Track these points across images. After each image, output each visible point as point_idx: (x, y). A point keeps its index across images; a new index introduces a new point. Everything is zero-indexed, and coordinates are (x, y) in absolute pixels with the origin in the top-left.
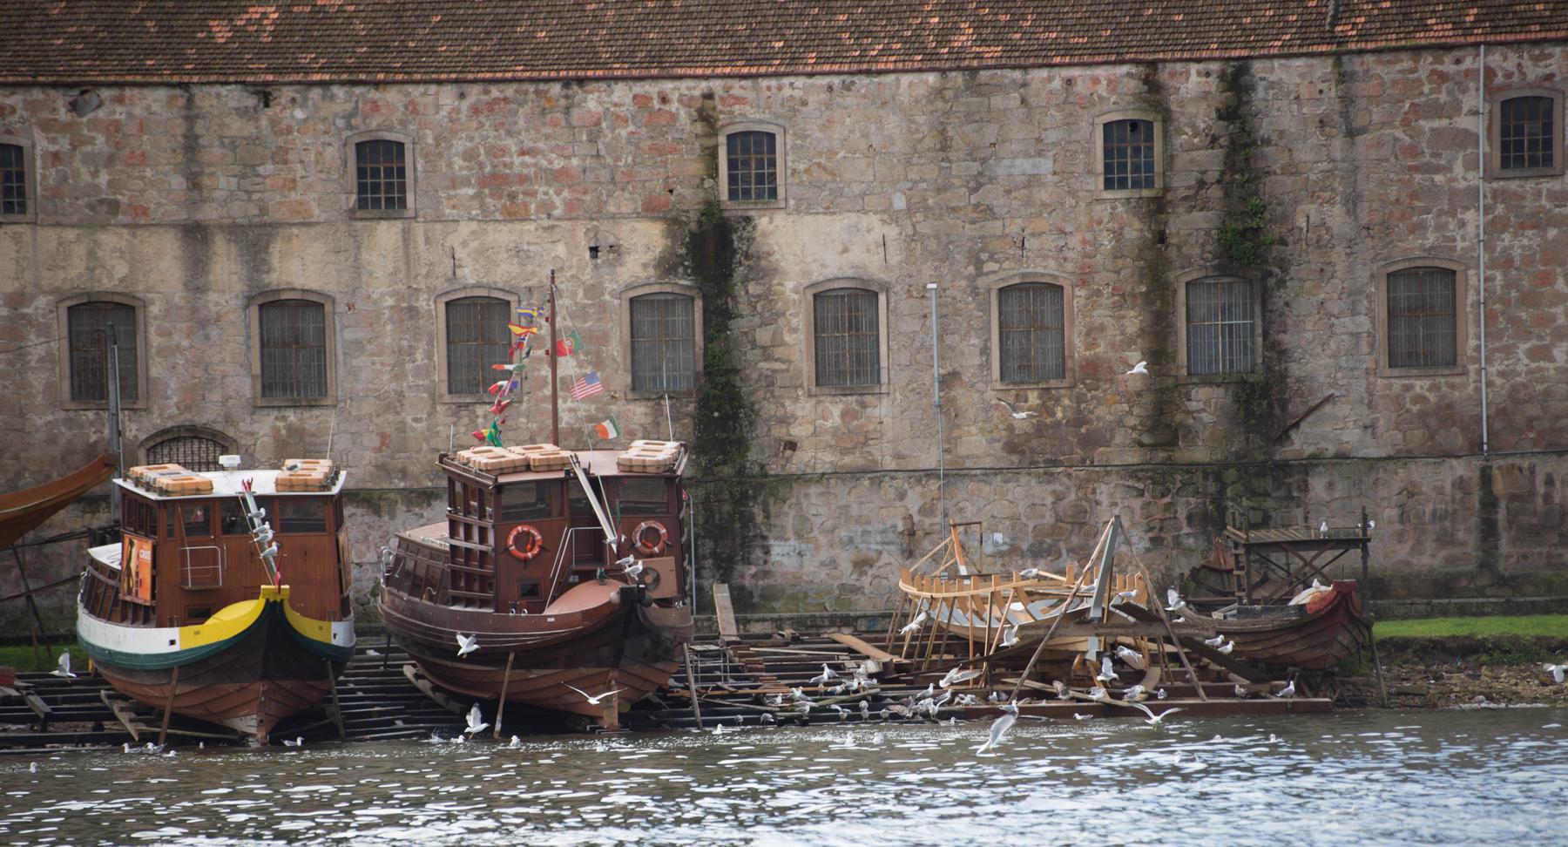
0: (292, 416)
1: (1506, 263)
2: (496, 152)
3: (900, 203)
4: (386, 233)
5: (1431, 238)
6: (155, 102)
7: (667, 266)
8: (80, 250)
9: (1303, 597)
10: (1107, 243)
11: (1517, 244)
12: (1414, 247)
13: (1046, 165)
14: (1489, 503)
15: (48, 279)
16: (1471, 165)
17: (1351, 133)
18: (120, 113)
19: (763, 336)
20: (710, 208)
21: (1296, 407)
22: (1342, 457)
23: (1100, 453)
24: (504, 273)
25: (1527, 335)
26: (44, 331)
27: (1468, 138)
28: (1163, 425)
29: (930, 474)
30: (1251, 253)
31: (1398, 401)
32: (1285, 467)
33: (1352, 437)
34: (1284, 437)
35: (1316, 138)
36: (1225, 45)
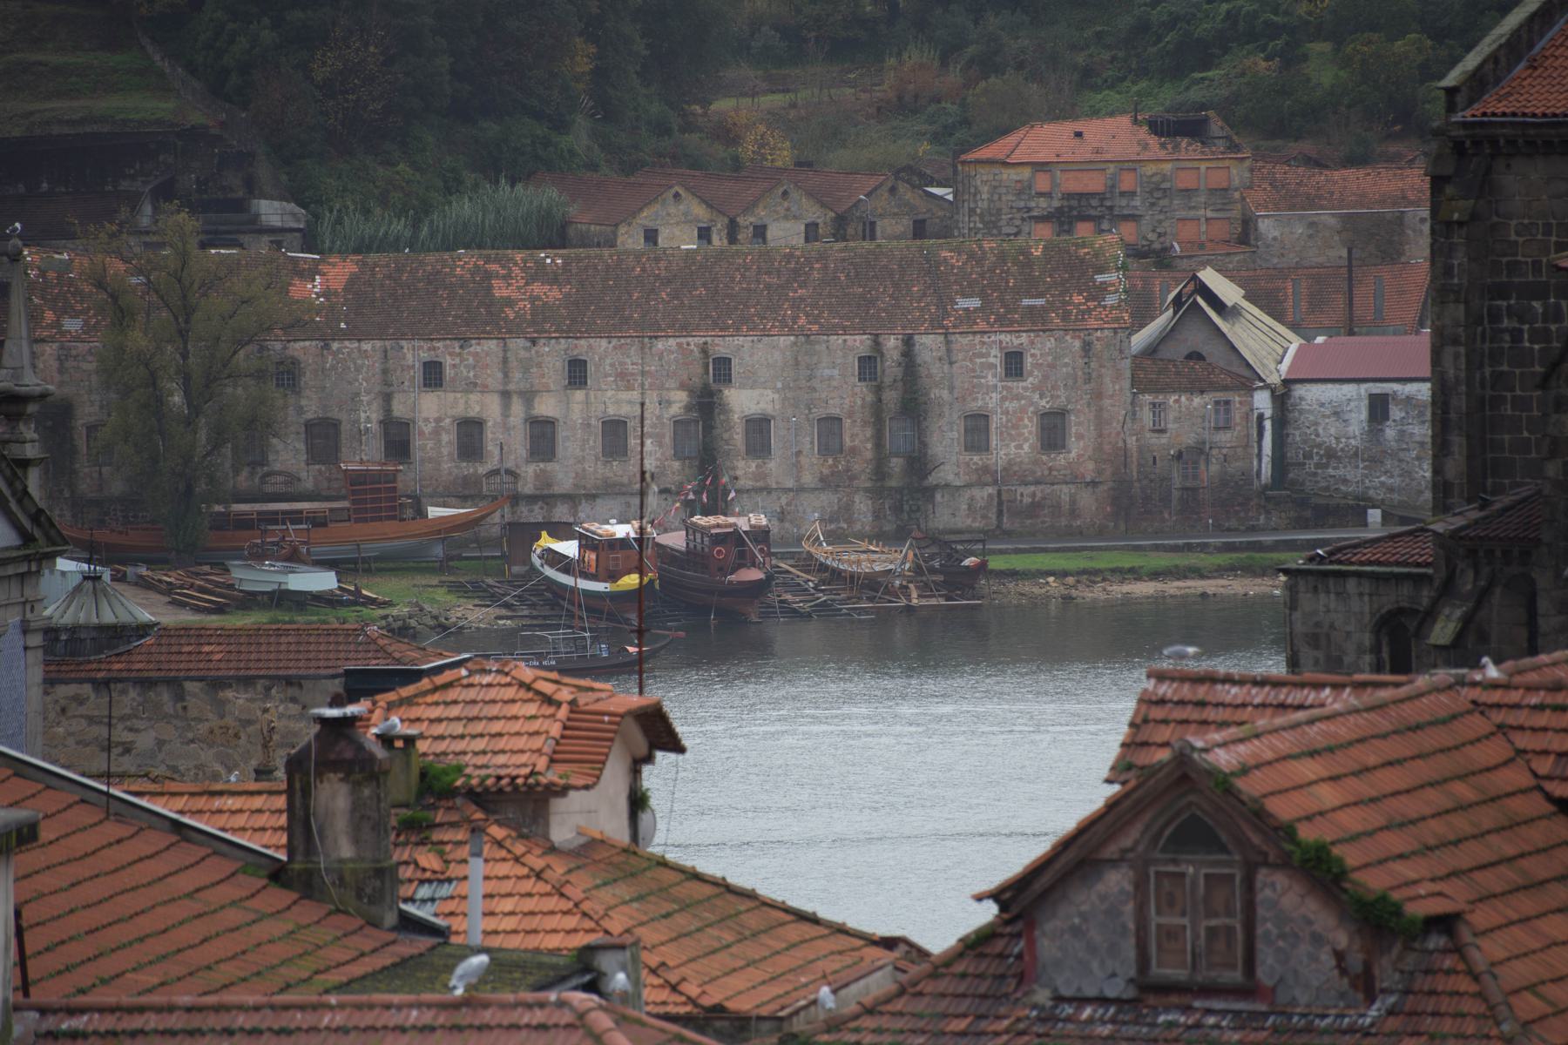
0: (542, 465)
1: (1007, 413)
2: (622, 364)
3: (779, 385)
4: (579, 395)
5: (980, 403)
6: (492, 345)
7: (688, 408)
8: (462, 401)
9: (967, 562)
10: (859, 402)
11: (1011, 406)
12: (974, 406)
13: (836, 372)
14: (1000, 503)
15: (450, 412)
16: (995, 376)
17: (951, 363)
18: (479, 349)
19: (726, 436)
20: (706, 386)
21: (930, 466)
22: (947, 485)
23: (856, 482)
25: (1013, 440)
26: (448, 432)
27: (993, 366)
28: (880, 472)
29: (790, 490)
30: (914, 407)
31: (968, 464)
32: (926, 489)
33: (951, 477)
34: (925, 477)
35: (938, 365)
36: (904, 328)
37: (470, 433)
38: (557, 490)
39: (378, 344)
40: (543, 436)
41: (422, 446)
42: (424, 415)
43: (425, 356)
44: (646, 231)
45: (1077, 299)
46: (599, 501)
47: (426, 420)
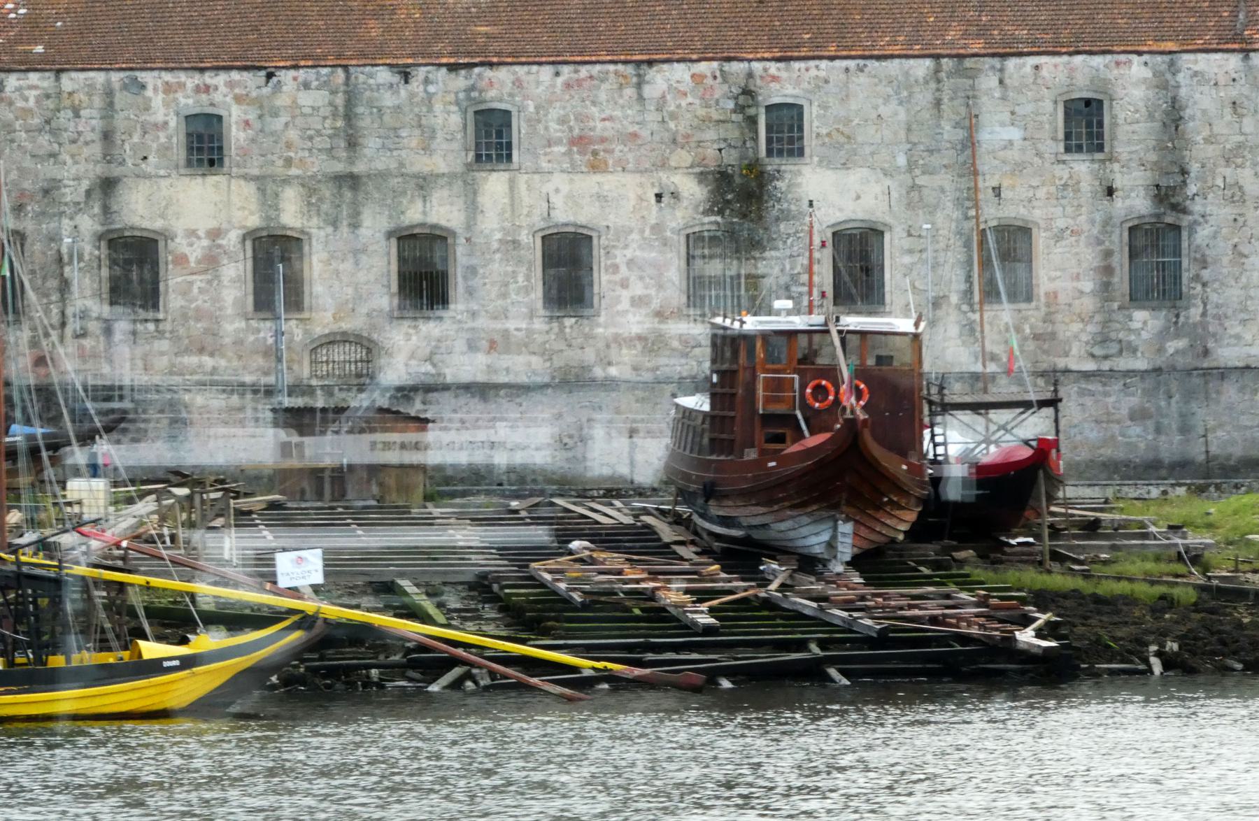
26: (232, 258)
39: (100, 77)
40: (424, 278)
43: (188, 102)
44: (150, 297)
46: (980, 168)
47: (192, 233)
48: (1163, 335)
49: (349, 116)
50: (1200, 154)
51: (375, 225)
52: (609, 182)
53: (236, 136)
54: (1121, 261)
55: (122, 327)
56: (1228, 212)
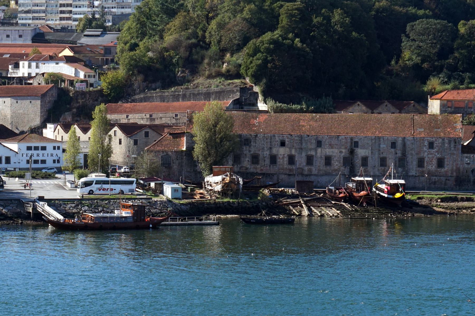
1: (429, 158)
11: (430, 156)
24: (331, 154)
27: (426, 146)
37: (291, 160)
38: (313, 173)
40: (310, 160)
41: (279, 161)
42: (280, 153)
45: (448, 130)
48: (402, 171)
49: (301, 140)
50: (408, 149)
51: (304, 154)
52: (333, 150)
53: (287, 143)
54: (397, 162)
55: (271, 166)
56: (411, 157)
